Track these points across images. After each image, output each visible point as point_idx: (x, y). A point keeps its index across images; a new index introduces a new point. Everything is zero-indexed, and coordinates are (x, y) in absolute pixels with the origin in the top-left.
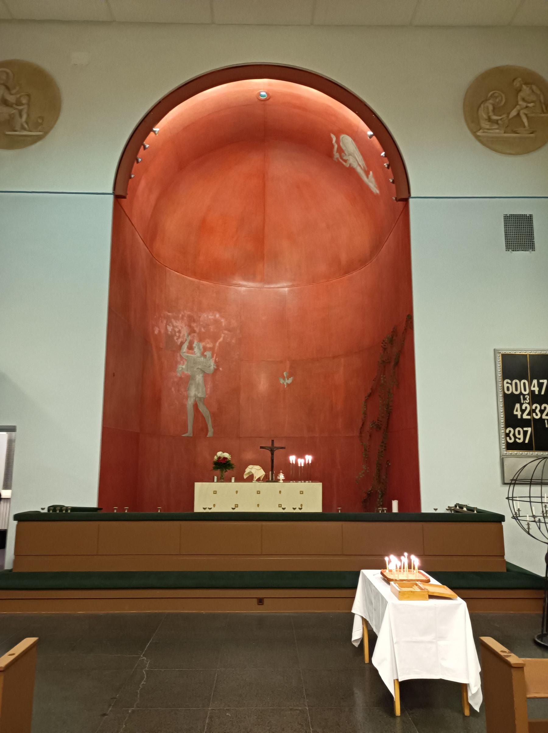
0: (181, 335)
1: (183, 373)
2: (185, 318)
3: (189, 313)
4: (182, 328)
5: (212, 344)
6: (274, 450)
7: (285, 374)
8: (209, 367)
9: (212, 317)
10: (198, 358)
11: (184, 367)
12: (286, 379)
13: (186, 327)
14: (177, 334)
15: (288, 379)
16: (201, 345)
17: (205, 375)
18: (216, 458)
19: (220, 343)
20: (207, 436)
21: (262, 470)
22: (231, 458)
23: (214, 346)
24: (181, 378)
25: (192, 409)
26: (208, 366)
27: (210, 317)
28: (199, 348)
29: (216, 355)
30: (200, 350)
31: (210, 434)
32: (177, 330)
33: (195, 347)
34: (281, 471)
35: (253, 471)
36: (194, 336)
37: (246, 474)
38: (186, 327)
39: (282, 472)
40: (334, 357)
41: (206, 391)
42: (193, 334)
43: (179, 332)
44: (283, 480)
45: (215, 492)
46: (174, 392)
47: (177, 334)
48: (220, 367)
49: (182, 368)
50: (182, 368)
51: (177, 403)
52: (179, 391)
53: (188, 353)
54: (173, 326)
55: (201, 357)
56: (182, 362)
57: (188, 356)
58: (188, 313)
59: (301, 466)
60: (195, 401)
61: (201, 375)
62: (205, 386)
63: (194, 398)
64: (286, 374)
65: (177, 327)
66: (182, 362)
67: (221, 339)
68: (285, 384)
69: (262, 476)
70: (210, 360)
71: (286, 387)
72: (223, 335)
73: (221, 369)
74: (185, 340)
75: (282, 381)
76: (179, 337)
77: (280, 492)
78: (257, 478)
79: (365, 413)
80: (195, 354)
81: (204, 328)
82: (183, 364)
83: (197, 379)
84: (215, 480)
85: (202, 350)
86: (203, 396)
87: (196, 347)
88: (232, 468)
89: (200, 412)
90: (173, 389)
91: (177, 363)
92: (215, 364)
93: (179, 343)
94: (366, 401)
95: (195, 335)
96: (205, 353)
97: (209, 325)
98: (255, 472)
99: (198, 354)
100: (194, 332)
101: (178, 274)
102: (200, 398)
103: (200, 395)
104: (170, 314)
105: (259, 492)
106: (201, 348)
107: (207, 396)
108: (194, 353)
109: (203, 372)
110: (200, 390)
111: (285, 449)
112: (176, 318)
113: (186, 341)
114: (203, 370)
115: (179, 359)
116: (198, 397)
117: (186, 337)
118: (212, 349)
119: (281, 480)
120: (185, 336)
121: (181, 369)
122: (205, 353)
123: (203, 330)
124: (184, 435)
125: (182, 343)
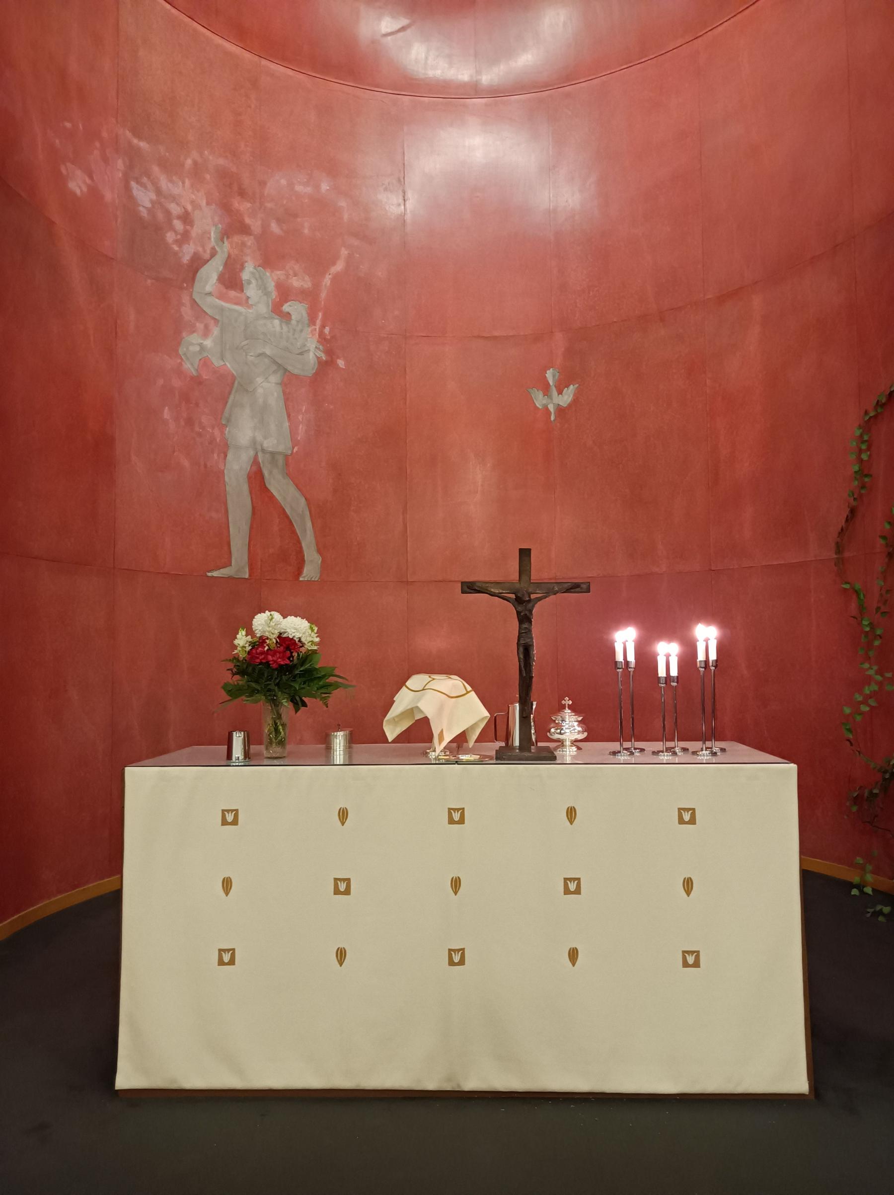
0: (195, 232)
1: (206, 363)
2: (208, 177)
3: (221, 161)
4: (196, 206)
5: (307, 278)
6: (533, 596)
7: (550, 376)
8: (301, 354)
9: (309, 190)
10: (261, 322)
11: (208, 343)
12: (554, 392)
13: (213, 207)
14: (178, 225)
15: (560, 392)
16: (271, 279)
17: (289, 381)
18: (242, 640)
19: (336, 278)
20: (301, 579)
21: (473, 693)
22: (317, 640)
23: (317, 286)
24: (197, 381)
25: (245, 488)
26: (297, 352)
27: (299, 188)
28: (263, 288)
29: (324, 315)
30: (267, 293)
31: (311, 571)
32: (175, 209)
33: (249, 282)
34: (568, 702)
35: (428, 707)
36: (243, 244)
37: (388, 720)
38: (213, 207)
39: (570, 707)
40: (722, 299)
41: (293, 432)
42: (237, 239)
43: (186, 218)
44: (575, 742)
45: (230, 818)
46: (172, 426)
47: (178, 225)
48: (338, 358)
49: (201, 345)
50: (202, 348)
51: (186, 463)
52: (190, 422)
53: (221, 297)
54: (158, 191)
55: (273, 318)
56: (200, 326)
57: (222, 310)
58: (215, 161)
59: (668, 677)
60: (255, 462)
61: (275, 379)
62: (289, 416)
63: (252, 453)
64: (554, 376)
65: (174, 199)
66: (200, 326)
67: (339, 267)
68: (551, 408)
69: (473, 727)
70: (301, 331)
71: (552, 418)
72: (344, 252)
73: (341, 363)
74: (208, 252)
75: (539, 399)
76: (185, 237)
77: (571, 814)
78: (448, 738)
79: (864, 472)
80: (250, 306)
81: (279, 221)
82: (206, 333)
83: (260, 391)
84: (238, 751)
85: (274, 295)
86: (281, 448)
87: (254, 281)
88: (327, 688)
89: (272, 497)
90: (167, 414)
91: (179, 328)
92: (321, 347)
93: (186, 259)
94: (868, 425)
95: (249, 241)
96: (286, 308)
97: (296, 216)
98: (441, 709)
99: (263, 308)
100: (244, 230)
101: (174, 11)
102: (273, 454)
103: (270, 444)
104: (143, 144)
105: (456, 817)
106: (270, 290)
107: (296, 449)
108: (245, 302)
109: (278, 365)
110: (273, 427)
111: (588, 591)
112: (171, 168)
113: (213, 254)
114: (280, 361)
115: (187, 312)
116: (263, 451)
117: (213, 242)
118: (309, 296)
119: (568, 743)
120: (209, 238)
121: (197, 348)
122: (286, 308)
123: (275, 228)
124: (215, 574)
125: (197, 263)
